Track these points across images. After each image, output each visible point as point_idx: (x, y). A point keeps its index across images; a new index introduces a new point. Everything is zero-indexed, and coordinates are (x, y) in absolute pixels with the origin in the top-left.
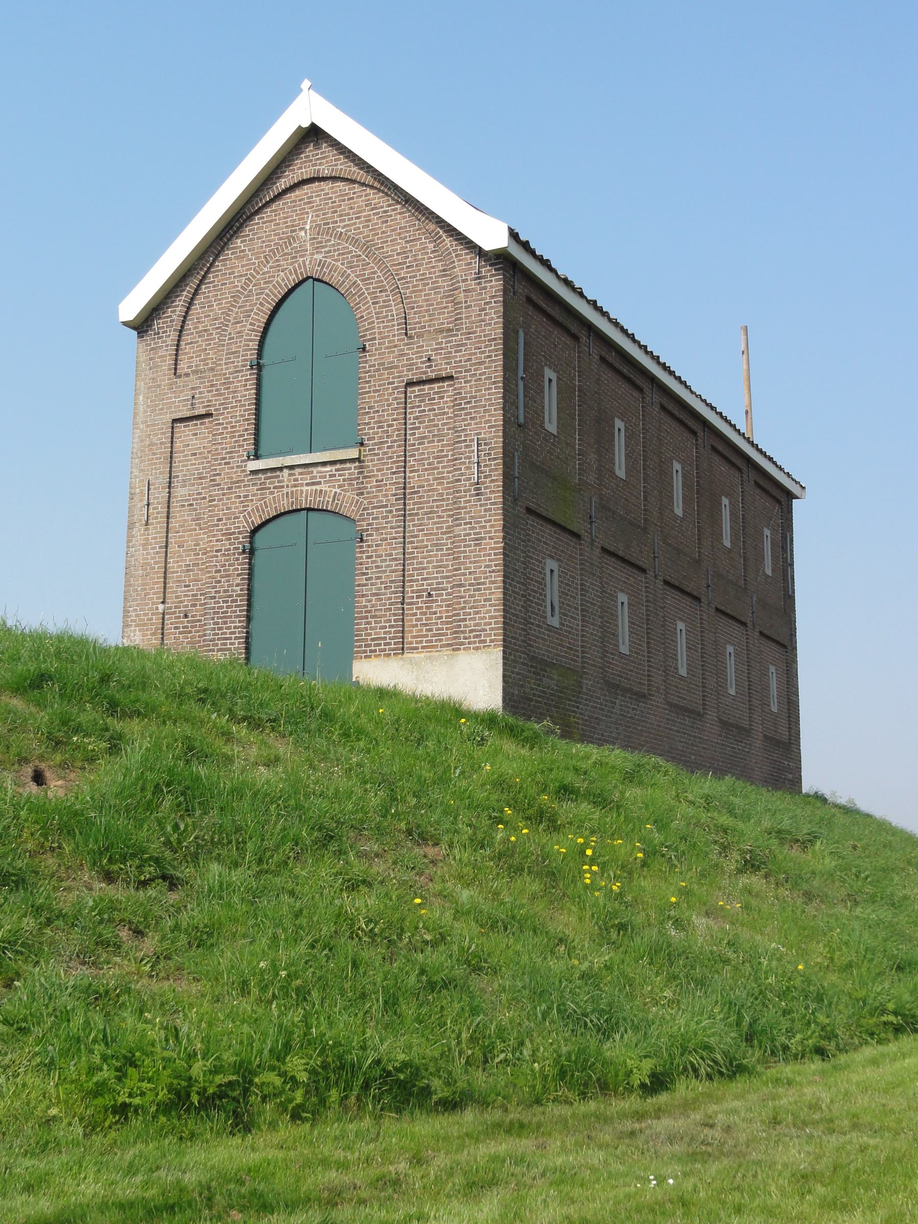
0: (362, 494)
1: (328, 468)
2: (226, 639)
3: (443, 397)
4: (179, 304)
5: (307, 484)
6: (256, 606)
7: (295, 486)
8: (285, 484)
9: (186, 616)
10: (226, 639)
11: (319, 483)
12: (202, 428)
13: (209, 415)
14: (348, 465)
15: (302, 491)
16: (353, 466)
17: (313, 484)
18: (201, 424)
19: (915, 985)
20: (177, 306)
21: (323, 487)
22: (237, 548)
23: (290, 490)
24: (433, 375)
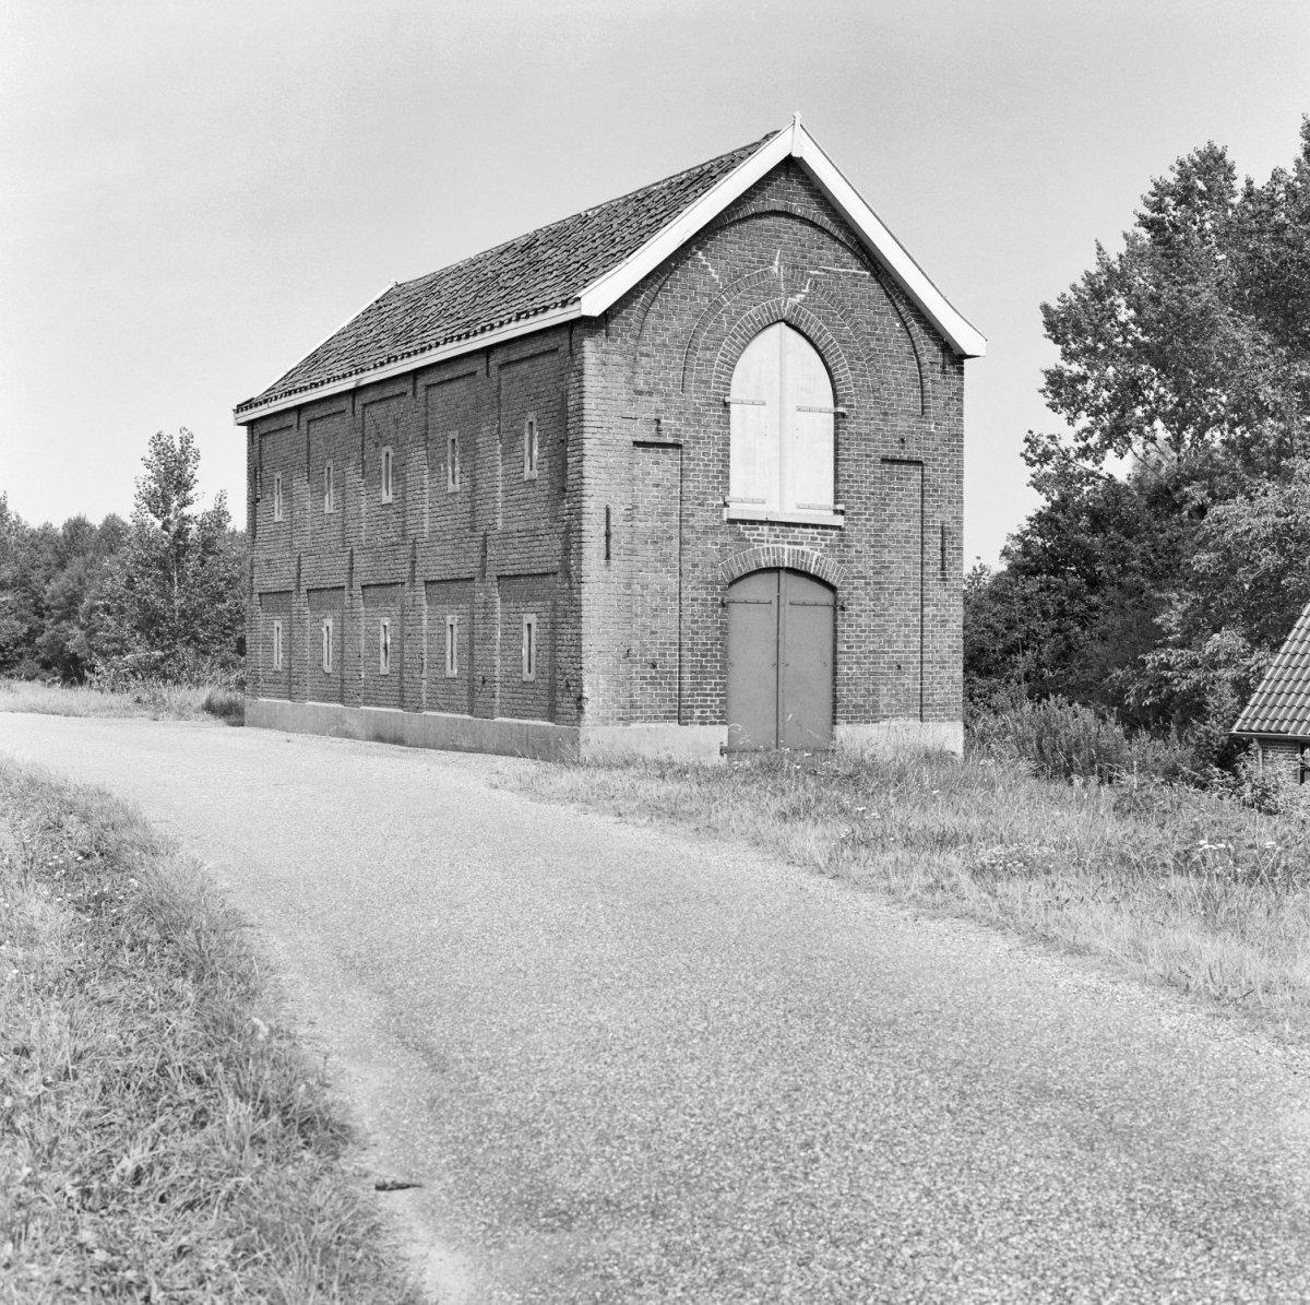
0: (843, 562)
1: (810, 530)
2: (707, 695)
3: (909, 479)
4: (824, 220)
5: (789, 543)
6: (829, 629)
7: (776, 542)
8: (765, 538)
9: (654, 666)
10: (707, 695)
11: (801, 544)
12: (668, 459)
13: (677, 446)
14: (829, 531)
15: (783, 549)
16: (834, 532)
17: (795, 543)
18: (664, 453)
19: (384, 1303)
20: (634, 308)
21: (806, 548)
22: (716, 600)
23: (770, 546)
24: (905, 457)
